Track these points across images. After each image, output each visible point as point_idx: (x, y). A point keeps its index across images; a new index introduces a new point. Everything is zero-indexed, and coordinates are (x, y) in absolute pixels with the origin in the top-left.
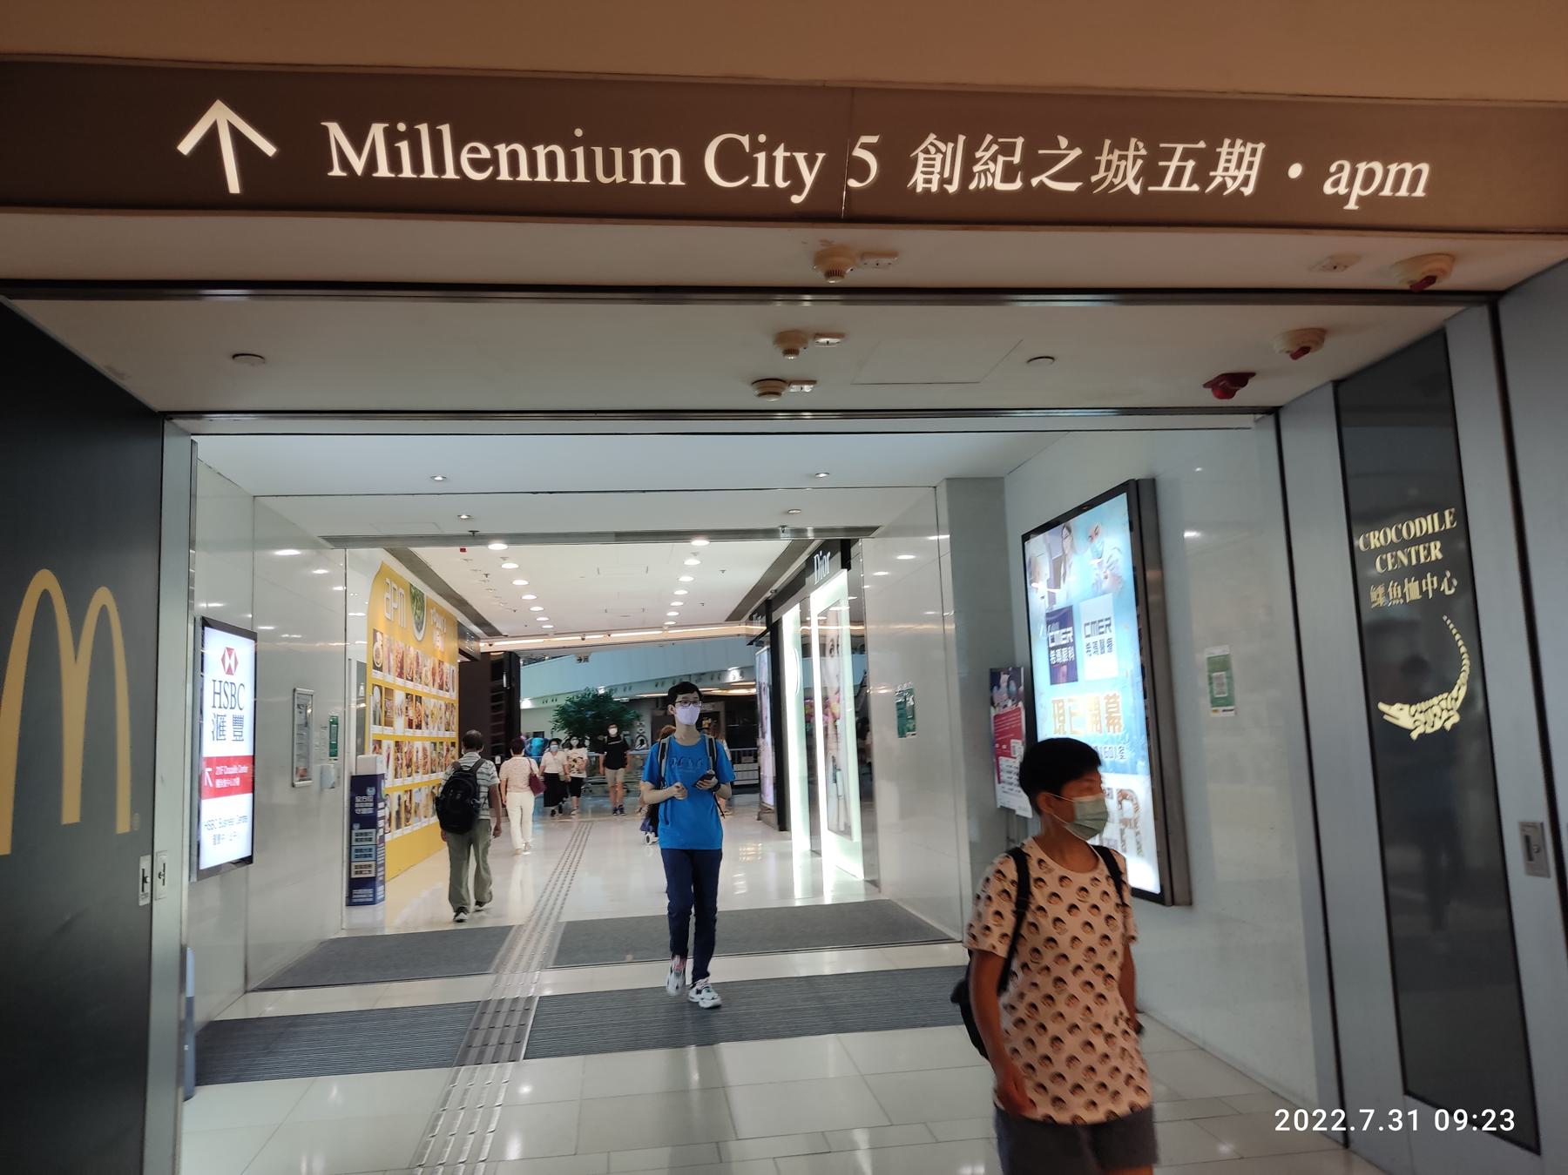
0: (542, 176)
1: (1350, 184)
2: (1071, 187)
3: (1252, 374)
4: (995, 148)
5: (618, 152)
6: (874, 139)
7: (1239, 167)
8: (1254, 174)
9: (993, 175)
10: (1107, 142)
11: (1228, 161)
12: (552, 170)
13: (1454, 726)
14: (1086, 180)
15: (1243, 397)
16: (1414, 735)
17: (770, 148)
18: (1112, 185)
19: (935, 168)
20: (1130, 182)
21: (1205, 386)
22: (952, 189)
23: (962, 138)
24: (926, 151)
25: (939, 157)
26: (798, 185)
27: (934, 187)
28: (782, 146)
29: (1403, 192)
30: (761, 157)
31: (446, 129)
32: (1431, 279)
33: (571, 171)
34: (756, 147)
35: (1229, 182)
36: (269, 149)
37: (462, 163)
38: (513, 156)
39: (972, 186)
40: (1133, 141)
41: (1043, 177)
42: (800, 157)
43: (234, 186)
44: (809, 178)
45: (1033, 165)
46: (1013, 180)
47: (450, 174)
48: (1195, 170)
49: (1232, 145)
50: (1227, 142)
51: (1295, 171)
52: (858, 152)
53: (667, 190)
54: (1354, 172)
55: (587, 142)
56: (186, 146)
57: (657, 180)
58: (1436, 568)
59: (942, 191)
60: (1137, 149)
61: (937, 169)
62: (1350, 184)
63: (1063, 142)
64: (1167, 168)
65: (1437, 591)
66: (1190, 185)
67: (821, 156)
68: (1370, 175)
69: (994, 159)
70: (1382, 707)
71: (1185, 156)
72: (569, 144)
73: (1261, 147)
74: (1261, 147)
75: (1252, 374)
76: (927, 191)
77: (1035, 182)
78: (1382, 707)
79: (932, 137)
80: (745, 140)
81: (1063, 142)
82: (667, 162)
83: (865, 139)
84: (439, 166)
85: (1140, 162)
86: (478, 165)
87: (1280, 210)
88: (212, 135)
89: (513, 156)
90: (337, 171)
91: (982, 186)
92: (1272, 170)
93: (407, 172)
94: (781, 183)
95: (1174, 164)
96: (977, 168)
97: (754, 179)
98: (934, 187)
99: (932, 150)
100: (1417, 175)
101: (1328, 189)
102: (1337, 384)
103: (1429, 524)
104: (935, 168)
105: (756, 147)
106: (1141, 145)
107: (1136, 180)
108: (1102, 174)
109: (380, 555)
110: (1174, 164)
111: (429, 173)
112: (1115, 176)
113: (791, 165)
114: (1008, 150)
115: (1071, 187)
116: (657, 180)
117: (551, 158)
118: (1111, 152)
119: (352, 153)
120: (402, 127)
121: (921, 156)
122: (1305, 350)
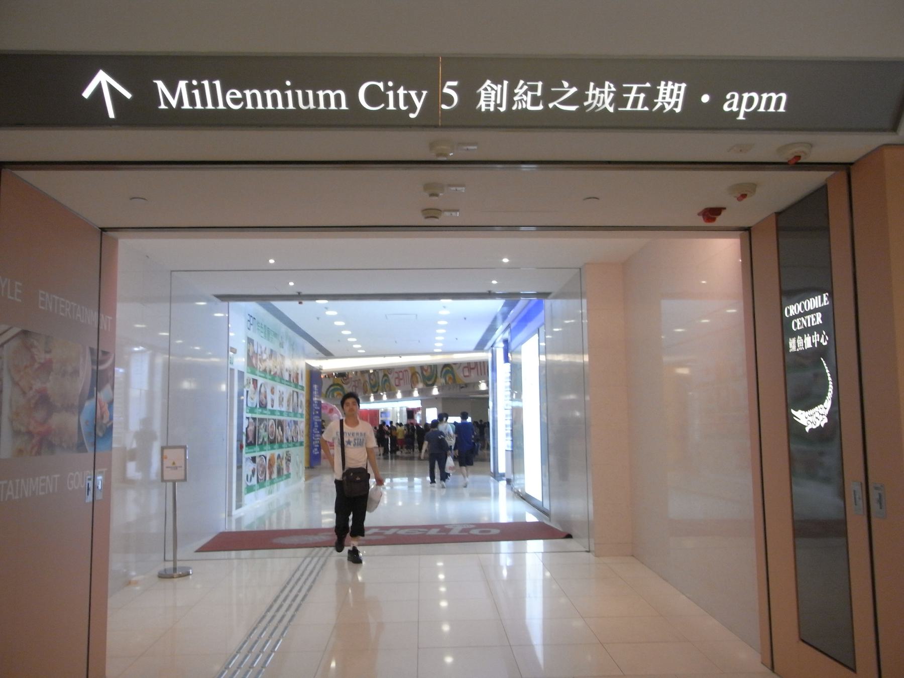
0: (270, 106)
1: (739, 106)
2: (573, 108)
3: (725, 208)
4: (526, 87)
5: (310, 93)
6: (455, 83)
7: (671, 97)
8: (681, 101)
9: (526, 102)
10: (592, 84)
11: (665, 94)
12: (275, 102)
13: (825, 424)
14: (581, 104)
15: (720, 221)
16: (807, 429)
17: (395, 89)
18: (597, 107)
19: (491, 96)
20: (607, 105)
21: (699, 214)
22: (503, 109)
23: (506, 83)
24: (486, 89)
25: (493, 93)
26: (413, 108)
27: (492, 109)
28: (402, 88)
29: (772, 109)
30: (391, 94)
31: (217, 83)
32: (799, 157)
33: (285, 103)
34: (387, 88)
35: (666, 105)
36: (128, 95)
37: (228, 100)
38: (254, 97)
39: (514, 108)
40: (607, 83)
41: (555, 103)
42: (413, 93)
43: (111, 115)
44: (419, 105)
45: (548, 96)
46: (538, 105)
47: (221, 106)
48: (645, 99)
49: (666, 85)
50: (663, 83)
51: (705, 98)
52: (446, 90)
53: (339, 112)
54: (741, 99)
55: (293, 88)
56: (87, 94)
57: (333, 107)
58: (817, 329)
59: (496, 110)
60: (610, 87)
61: (493, 99)
62: (739, 106)
63: (566, 84)
64: (628, 98)
65: (819, 343)
66: (643, 107)
67: (425, 93)
68: (751, 101)
69: (525, 93)
70: (793, 412)
71: (639, 91)
72: (283, 89)
73: (684, 85)
74: (684, 85)
75: (725, 208)
76: (488, 111)
77: (551, 105)
78: (793, 412)
79: (488, 82)
80: (381, 85)
81: (566, 84)
82: (338, 97)
83: (449, 83)
84: (215, 102)
85: (612, 95)
86: (236, 101)
87: (696, 119)
88: (99, 88)
89: (254, 97)
90: (163, 106)
91: (520, 108)
92: (691, 98)
93: (199, 106)
94: (402, 107)
95: (632, 96)
96: (516, 98)
97: (387, 105)
98: (492, 109)
99: (489, 89)
100: (779, 100)
101: (726, 108)
102: (778, 214)
103: (815, 302)
104: (491, 96)
105: (387, 88)
106: (612, 85)
107: (610, 105)
108: (590, 101)
109: (253, 307)
110: (632, 96)
111: (210, 106)
112: (598, 102)
113: (408, 98)
114: (534, 88)
115: (573, 108)
116: (333, 107)
117: (274, 97)
118: (594, 89)
119: (174, 95)
120: (195, 83)
121: (483, 92)
122: (744, 196)
